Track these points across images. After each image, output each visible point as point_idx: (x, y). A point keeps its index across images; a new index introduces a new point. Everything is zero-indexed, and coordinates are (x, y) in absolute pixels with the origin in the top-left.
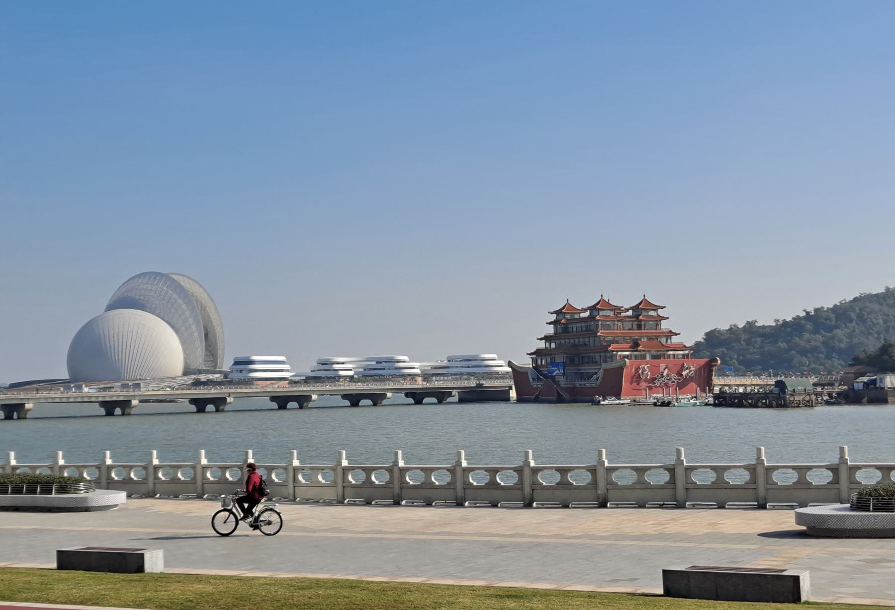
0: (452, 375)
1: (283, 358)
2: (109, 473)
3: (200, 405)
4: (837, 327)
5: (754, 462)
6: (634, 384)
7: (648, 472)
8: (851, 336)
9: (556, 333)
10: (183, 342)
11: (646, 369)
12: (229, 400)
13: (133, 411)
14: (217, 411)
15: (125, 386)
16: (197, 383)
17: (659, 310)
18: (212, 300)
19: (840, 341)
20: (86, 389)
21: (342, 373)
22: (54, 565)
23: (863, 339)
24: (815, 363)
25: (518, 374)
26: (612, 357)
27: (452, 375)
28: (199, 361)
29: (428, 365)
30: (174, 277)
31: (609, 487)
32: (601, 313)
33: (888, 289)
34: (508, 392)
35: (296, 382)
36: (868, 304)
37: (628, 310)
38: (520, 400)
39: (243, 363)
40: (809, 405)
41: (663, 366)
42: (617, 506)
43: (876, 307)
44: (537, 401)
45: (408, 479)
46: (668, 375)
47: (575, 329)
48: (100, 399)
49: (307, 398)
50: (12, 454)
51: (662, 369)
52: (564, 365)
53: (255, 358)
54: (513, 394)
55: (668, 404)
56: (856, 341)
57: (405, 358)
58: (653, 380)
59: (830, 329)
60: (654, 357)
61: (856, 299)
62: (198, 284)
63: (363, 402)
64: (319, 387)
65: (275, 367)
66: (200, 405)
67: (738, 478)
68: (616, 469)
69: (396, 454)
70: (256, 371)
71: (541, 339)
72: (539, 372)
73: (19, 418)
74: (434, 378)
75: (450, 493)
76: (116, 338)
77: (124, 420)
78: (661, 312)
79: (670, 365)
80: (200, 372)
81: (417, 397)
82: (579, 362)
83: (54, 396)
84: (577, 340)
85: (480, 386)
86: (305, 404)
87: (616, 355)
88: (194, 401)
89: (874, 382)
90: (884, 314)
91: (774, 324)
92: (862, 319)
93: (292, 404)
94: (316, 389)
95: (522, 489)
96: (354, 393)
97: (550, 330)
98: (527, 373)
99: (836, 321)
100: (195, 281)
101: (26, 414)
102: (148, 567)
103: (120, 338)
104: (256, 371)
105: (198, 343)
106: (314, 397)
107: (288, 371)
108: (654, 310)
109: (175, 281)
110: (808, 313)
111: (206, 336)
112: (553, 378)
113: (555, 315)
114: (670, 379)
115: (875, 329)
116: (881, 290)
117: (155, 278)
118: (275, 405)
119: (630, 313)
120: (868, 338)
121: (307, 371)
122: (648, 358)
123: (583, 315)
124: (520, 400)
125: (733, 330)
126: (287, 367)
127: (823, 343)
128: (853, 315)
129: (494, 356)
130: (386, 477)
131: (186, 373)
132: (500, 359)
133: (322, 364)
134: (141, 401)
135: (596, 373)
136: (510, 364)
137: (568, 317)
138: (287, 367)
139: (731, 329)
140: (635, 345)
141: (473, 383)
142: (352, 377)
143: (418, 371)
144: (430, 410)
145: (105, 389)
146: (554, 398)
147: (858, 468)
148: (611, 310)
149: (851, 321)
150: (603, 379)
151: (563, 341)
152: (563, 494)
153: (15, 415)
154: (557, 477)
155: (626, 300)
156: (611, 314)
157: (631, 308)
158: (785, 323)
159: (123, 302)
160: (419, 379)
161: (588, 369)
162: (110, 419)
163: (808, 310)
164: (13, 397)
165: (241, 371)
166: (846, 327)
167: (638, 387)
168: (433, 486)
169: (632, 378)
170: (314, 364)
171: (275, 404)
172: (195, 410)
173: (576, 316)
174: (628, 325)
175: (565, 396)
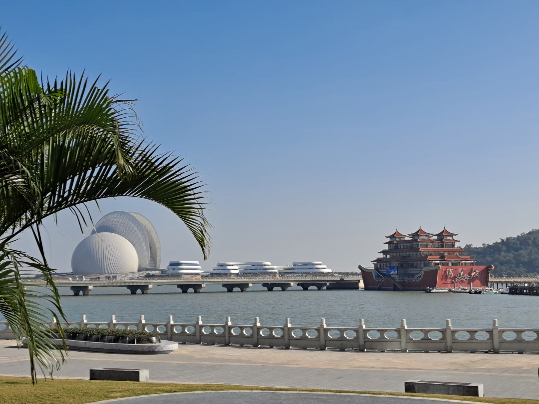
0: (296, 273)
1: (197, 262)
4: (521, 249)
6: (444, 280)
7: (524, 333)
8: (530, 254)
9: (390, 249)
10: (138, 252)
11: (451, 271)
15: (109, 278)
18: (154, 228)
19: (524, 257)
21: (232, 271)
22: (89, 378)
24: (509, 270)
25: (365, 273)
26: (427, 264)
27: (296, 273)
28: (147, 264)
29: (282, 267)
30: (132, 214)
32: (420, 237)
34: (357, 284)
38: (367, 288)
39: (175, 265)
41: (460, 270)
44: (379, 289)
46: (463, 275)
47: (402, 247)
48: (127, 284)
49: (247, 285)
50: (85, 316)
51: (460, 271)
52: (398, 268)
54: (361, 285)
55: (480, 293)
56: (533, 257)
57: (269, 263)
58: (454, 278)
59: (517, 250)
61: (530, 233)
63: (235, 289)
64: (151, 280)
68: (411, 331)
70: (183, 269)
71: (380, 253)
76: (100, 249)
78: (455, 238)
79: (464, 269)
80: (147, 269)
81: (270, 287)
82: (406, 266)
84: (401, 254)
86: (245, 289)
87: (431, 263)
91: (482, 246)
92: (534, 243)
93: (191, 290)
94: (252, 280)
96: (270, 283)
97: (386, 247)
99: (520, 245)
100: (141, 215)
104: (183, 269)
105: (146, 253)
106: (251, 285)
107: (200, 269)
109: (133, 217)
110: (503, 240)
111: (151, 248)
112: (390, 276)
113: (389, 238)
114: (465, 278)
117: (121, 215)
118: (180, 290)
119: (436, 238)
122: (450, 265)
123: (406, 239)
124: (367, 288)
126: (199, 267)
128: (530, 242)
131: (140, 270)
133: (221, 266)
136: (360, 267)
137: (398, 239)
138: (199, 267)
140: (442, 257)
141: (337, 278)
142: (238, 274)
143: (276, 271)
145: (96, 279)
146: (392, 288)
147: (504, 331)
148: (426, 236)
149: (529, 245)
150: (424, 275)
154: (378, 335)
155: (434, 230)
156: (426, 238)
157: (437, 235)
158: (489, 246)
159: (103, 228)
161: (411, 271)
162: (134, 296)
163: (503, 239)
165: (174, 269)
166: (526, 249)
167: (446, 282)
169: (443, 276)
170: (215, 266)
172: (267, 289)
173: (402, 239)
175: (399, 287)
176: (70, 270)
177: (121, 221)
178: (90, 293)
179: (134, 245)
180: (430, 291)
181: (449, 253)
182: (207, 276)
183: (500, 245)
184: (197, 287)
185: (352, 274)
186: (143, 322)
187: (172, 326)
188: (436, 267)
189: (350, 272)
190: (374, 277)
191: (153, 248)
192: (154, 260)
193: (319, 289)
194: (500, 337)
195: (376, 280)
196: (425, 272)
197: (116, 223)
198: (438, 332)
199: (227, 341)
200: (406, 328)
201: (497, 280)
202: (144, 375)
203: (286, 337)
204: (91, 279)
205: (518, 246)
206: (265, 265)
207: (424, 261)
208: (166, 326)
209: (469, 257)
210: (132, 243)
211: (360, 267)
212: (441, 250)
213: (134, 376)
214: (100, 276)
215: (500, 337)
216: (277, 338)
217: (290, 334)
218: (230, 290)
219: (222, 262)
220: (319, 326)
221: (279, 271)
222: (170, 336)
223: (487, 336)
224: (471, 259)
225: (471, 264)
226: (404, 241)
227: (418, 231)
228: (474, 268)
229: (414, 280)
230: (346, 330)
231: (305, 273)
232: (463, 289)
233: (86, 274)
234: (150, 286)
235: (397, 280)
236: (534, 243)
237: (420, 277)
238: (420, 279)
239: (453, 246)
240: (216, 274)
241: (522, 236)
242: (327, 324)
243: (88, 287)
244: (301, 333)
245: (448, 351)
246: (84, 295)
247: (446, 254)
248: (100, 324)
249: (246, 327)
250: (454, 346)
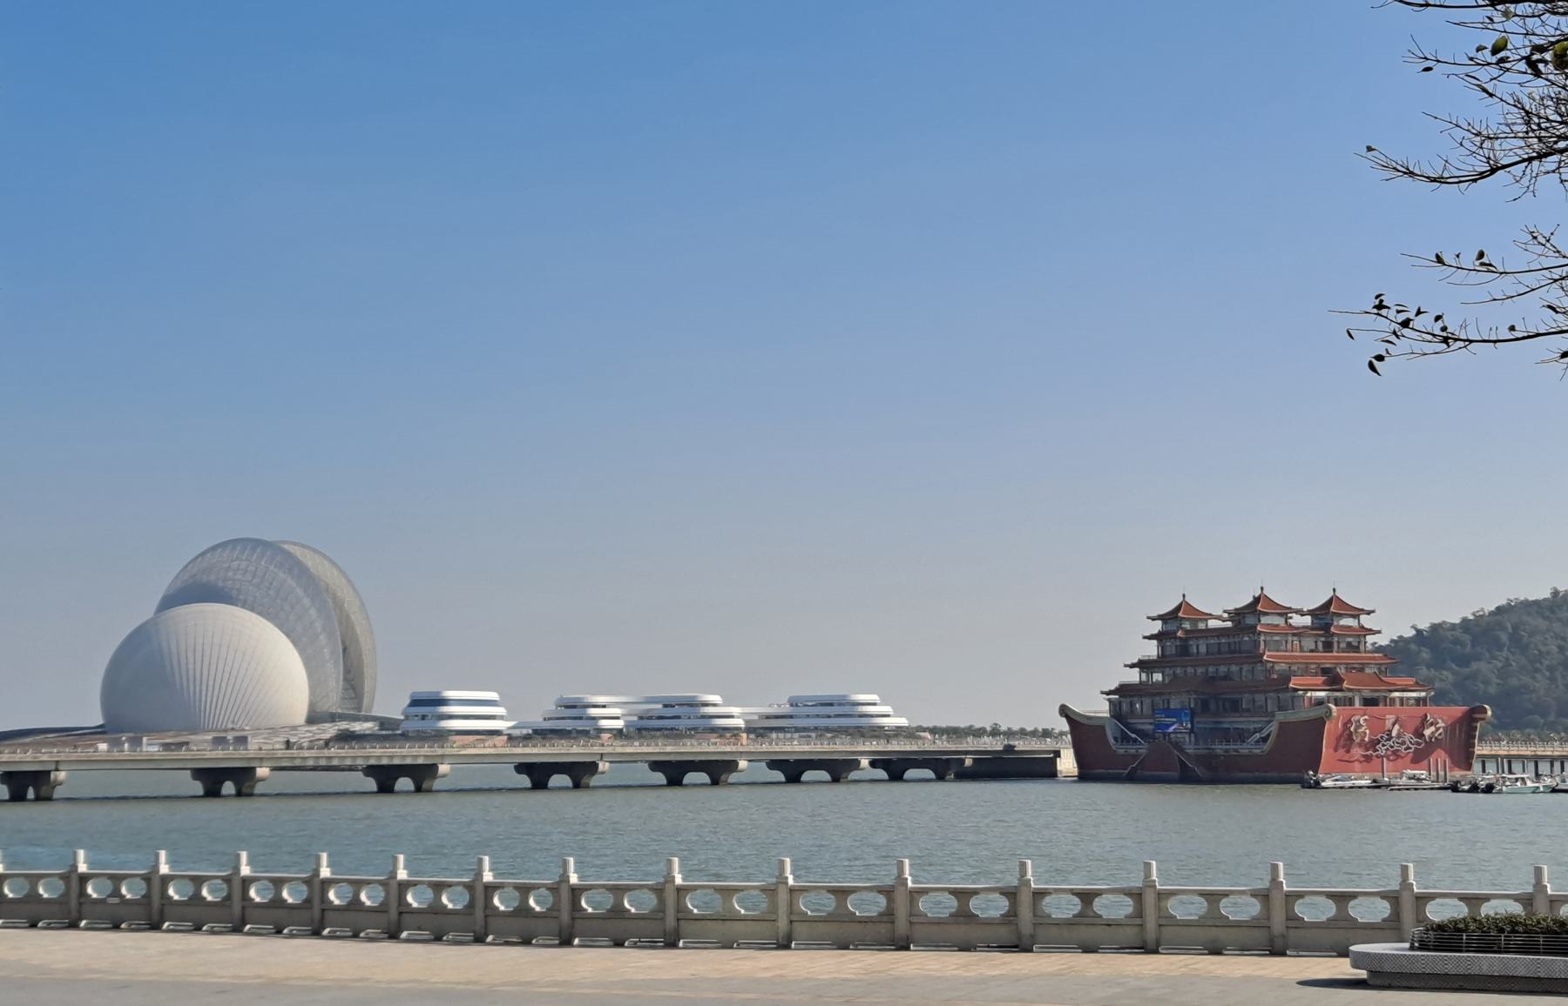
0: (797, 730)
1: (493, 696)
2: (245, 891)
3: (674, 772)
4: (1478, 658)
5: (1530, 889)
6: (1341, 751)
10: (307, 662)
11: (1362, 721)
13: (259, 788)
14: (419, 789)
15: (219, 741)
17: (1363, 618)
18: (355, 590)
19: (1486, 682)
21: (604, 723)
23: (1526, 679)
25: (1082, 730)
27: (797, 730)
31: (1291, 924)
32: (1264, 620)
33: (1556, 593)
34: (1052, 762)
36: (1525, 618)
38: (1088, 773)
39: (428, 703)
41: (1390, 719)
42: (808, 947)
43: (1541, 623)
44: (1132, 778)
45: (583, 904)
46: (1399, 736)
47: (1203, 649)
49: (731, 766)
51: (1388, 724)
53: (450, 694)
54: (1067, 763)
55: (1489, 789)
56: (1514, 682)
58: (1374, 744)
59: (1464, 661)
60: (1369, 702)
62: (330, 560)
63: (690, 778)
65: (483, 710)
67: (992, 907)
69: (565, 864)
70: (451, 717)
71: (1132, 666)
73: (38, 799)
74: (774, 735)
75: (1259, 935)
77: (422, 803)
78: (1365, 620)
79: (1402, 717)
80: (333, 718)
84: (1178, 671)
85: (1009, 749)
86: (723, 777)
88: (522, 768)
90: (1557, 636)
92: (1515, 639)
93: (558, 780)
95: (663, 919)
96: (792, 758)
97: (1152, 650)
98: (1102, 728)
99: (1473, 646)
100: (315, 551)
101: (253, 787)
103: (199, 654)
104: (451, 717)
106: (743, 764)
107: (501, 718)
108: (1354, 616)
109: (289, 555)
110: (1419, 632)
111: (345, 650)
113: (1159, 623)
115: (1546, 663)
116: (1545, 594)
119: (1307, 620)
120: (1534, 678)
121: (537, 719)
123: (1213, 624)
124: (1088, 773)
126: (500, 711)
128: (1504, 637)
130: (650, 901)
131: (312, 719)
132: (884, 703)
133: (567, 707)
134: (274, 769)
136: (1064, 711)
137: (1187, 626)
138: (500, 711)
140: (1333, 680)
141: (996, 745)
142: (620, 731)
143: (740, 723)
144: (816, 793)
146: (1175, 774)
148: (1280, 615)
149: (1500, 648)
150: (1278, 735)
151: (1178, 671)
152: (962, 932)
153: (31, 794)
154: (830, 903)
155: (1300, 595)
156: (1280, 621)
162: (213, 805)
164: (23, 758)
165: (424, 717)
168: (444, 911)
169: (1338, 739)
170: (550, 707)
173: (1201, 626)
174: (1309, 643)
176: (97, 719)
177: (252, 568)
178: (58, 793)
179: (295, 643)
180: (1317, 785)
181: (1349, 668)
182: (527, 738)
183: (1413, 647)
185: (1046, 733)
186: (83, 868)
187: (166, 880)
188: (1320, 711)
189: (963, 725)
190: (1112, 741)
192: (354, 688)
193: (941, 777)
196: (1282, 726)
197: (238, 577)
198: (1378, 899)
199: (156, 917)
200: (791, 882)
201: (1503, 749)
204: (167, 747)
205: (1468, 649)
206: (706, 705)
207: (1277, 691)
208: (147, 879)
209: (1411, 681)
211: (1064, 711)
214: (193, 737)
216: (453, 912)
217: (82, 893)
219: (571, 695)
220: (774, 880)
221: (747, 722)
224: (1418, 686)
225: (1418, 701)
226: (1208, 630)
227: (1178, 608)
228: (1432, 712)
229: (1244, 749)
230: (125, 877)
231: (827, 729)
232: (1413, 777)
233: (152, 730)
234: (443, 768)
235: (1190, 749)
236: (1515, 639)
237: (1265, 740)
238: (1266, 747)
240: (553, 731)
241: (1479, 618)
242: (796, 878)
243: (254, 769)
244: (608, 900)
245: (1147, 948)
246: (239, 794)
247: (1341, 671)
248: (1487, 898)
249: (368, 882)
250: (1294, 935)
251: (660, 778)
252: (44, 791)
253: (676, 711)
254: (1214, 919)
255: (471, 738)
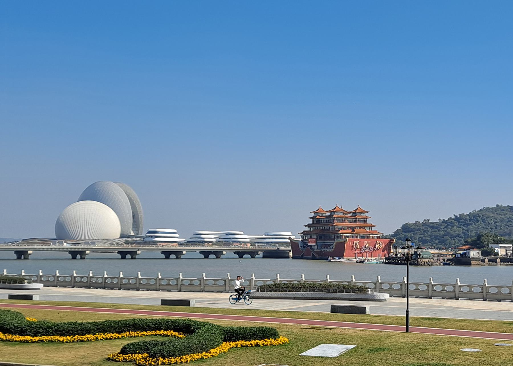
9: (313, 223)
12: (138, 252)
13: (86, 257)
14: (132, 258)
16: (127, 243)
20: (65, 244)
21: (206, 240)
22: (7, 298)
25: (293, 244)
26: (340, 237)
27: (267, 243)
33: (498, 206)
35: (181, 244)
36: (487, 213)
37: (350, 213)
38: (294, 258)
40: (429, 264)
43: (491, 215)
44: (302, 258)
46: (368, 247)
48: (69, 250)
54: (291, 254)
58: (361, 249)
63: (211, 256)
65: (169, 236)
66: (123, 254)
70: (214, 238)
71: (306, 226)
72: (304, 243)
79: (369, 242)
81: (240, 254)
83: (44, 247)
87: (342, 236)
89: (465, 254)
91: (438, 222)
92: (483, 221)
93: (173, 256)
96: (212, 251)
97: (311, 221)
102: (34, 299)
110: (456, 216)
111: (134, 217)
118: (163, 256)
122: (359, 238)
124: (294, 258)
125: (417, 224)
126: (177, 235)
127: (463, 233)
129: (242, 233)
131: (121, 237)
135: (332, 245)
138: (177, 235)
139: (416, 223)
143: (248, 240)
144: (247, 260)
146: (311, 257)
149: (478, 221)
153: (23, 257)
155: (350, 208)
160: (249, 245)
161: (328, 242)
162: (74, 261)
164: (23, 247)
171: (163, 255)
172: (238, 257)
173: (324, 215)
175: (317, 256)
184: (178, 254)
191: (136, 216)
193: (253, 257)
194: (487, 290)
195: (301, 249)
202: (367, 311)
203: (119, 282)
210: (115, 212)
212: (354, 225)
213: (186, 303)
215: (487, 290)
218: (206, 257)
222: (39, 280)
223: (426, 288)
235: (315, 250)
238: (333, 249)
239: (364, 221)
246: (81, 258)
251: (203, 256)
252: (83, 257)
253: (230, 236)
254: (499, 293)
255: (166, 243)
